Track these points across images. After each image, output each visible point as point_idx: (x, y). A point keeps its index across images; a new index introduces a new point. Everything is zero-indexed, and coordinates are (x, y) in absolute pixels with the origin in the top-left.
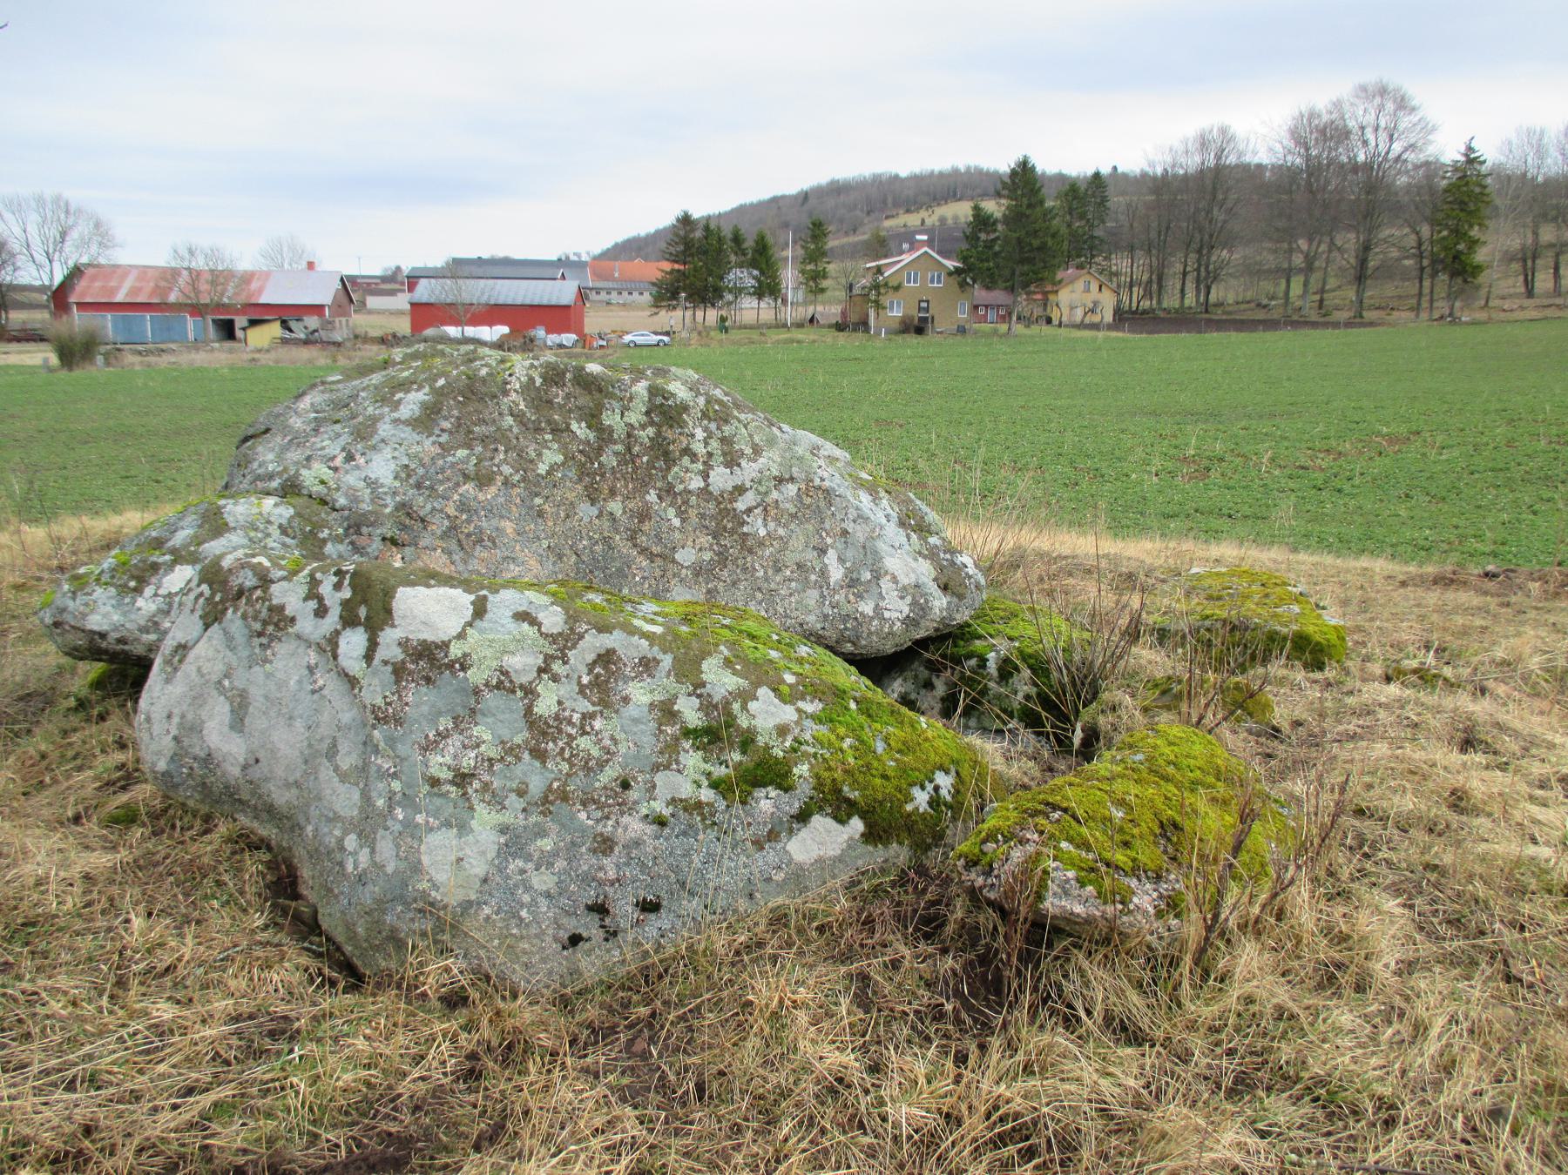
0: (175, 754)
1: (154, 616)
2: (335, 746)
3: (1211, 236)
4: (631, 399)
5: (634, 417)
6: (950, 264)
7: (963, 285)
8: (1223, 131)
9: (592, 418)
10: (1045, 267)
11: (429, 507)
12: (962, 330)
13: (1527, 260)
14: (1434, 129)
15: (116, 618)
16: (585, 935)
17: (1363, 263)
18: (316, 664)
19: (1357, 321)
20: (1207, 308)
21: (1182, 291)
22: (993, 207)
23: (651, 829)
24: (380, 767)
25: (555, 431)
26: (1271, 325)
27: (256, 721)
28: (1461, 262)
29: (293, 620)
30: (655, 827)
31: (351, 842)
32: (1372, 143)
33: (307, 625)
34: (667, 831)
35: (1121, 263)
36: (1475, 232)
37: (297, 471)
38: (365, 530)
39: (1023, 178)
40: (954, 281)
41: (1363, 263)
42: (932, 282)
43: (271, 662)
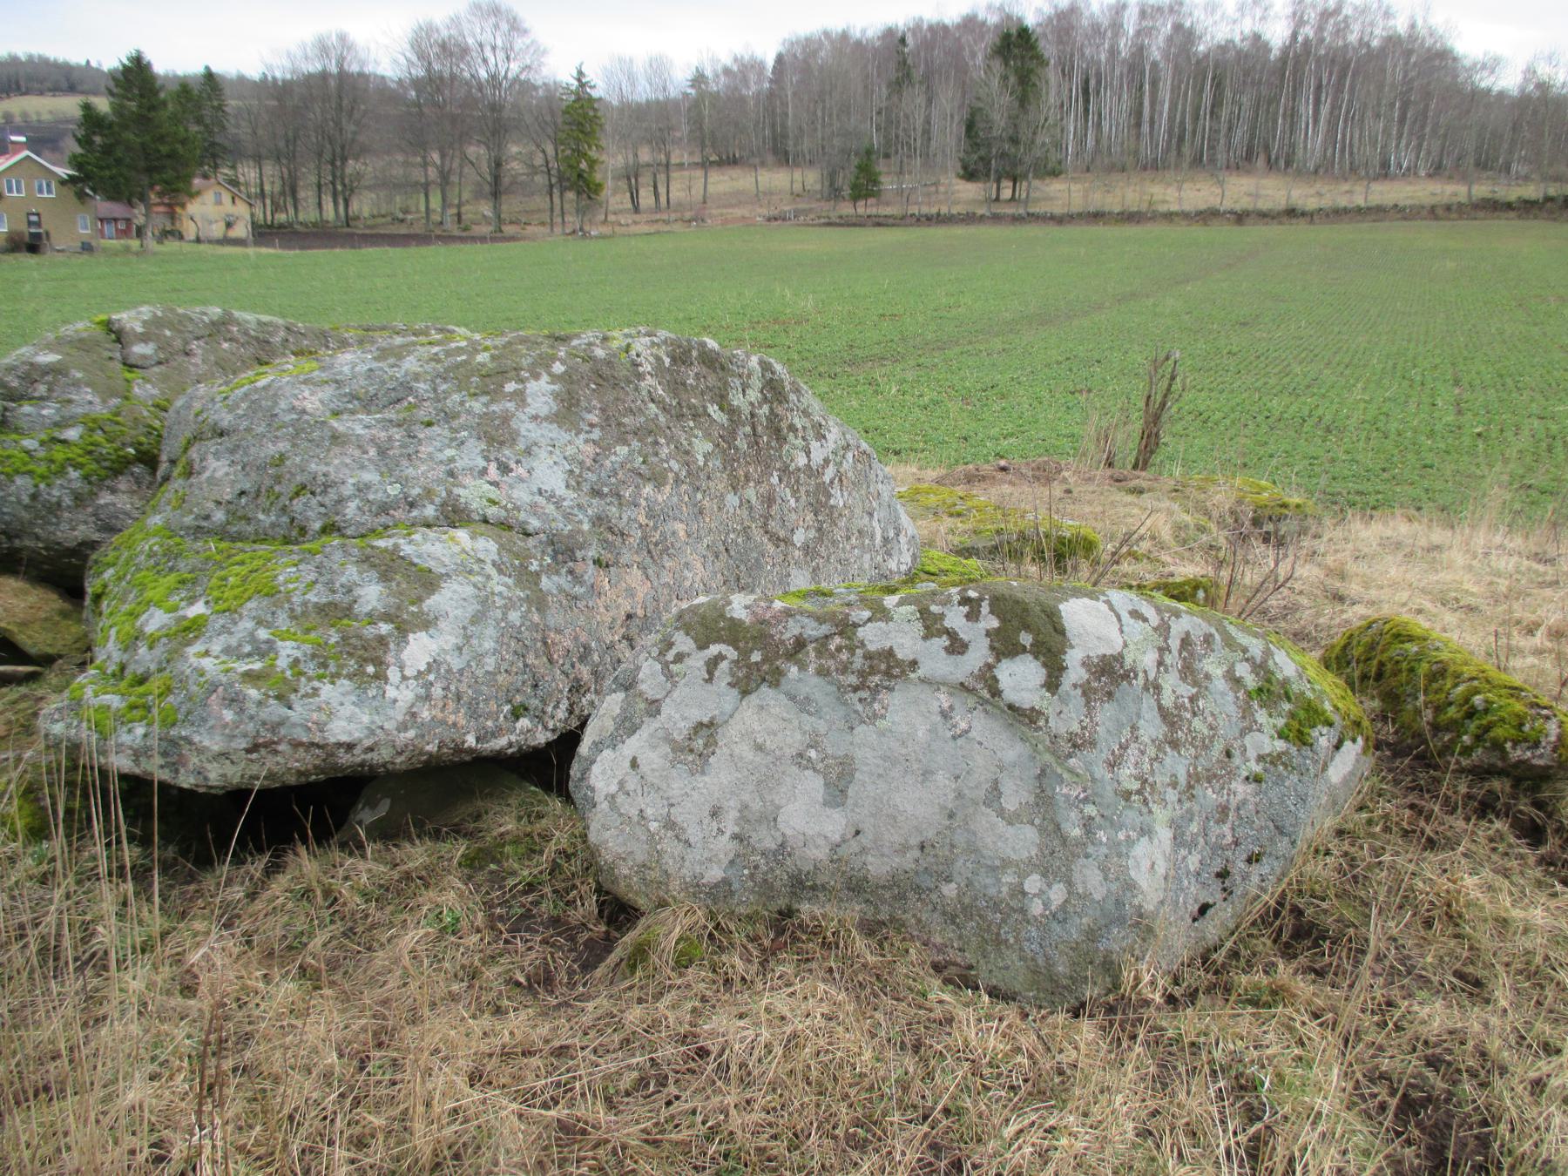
0: (737, 856)
1: (413, 705)
2: (996, 788)
3: (343, 148)
4: (749, 376)
5: (754, 395)
6: (63, 172)
7: (81, 196)
8: (342, 38)
9: (722, 400)
10: (178, 178)
11: (625, 517)
12: (87, 248)
13: (631, 176)
14: (545, 52)
15: (366, 719)
16: (1211, 901)
17: (497, 179)
18: (951, 708)
19: (498, 237)
20: (349, 221)
21: (320, 205)
22: (103, 105)
23: (1251, 787)
24: (1067, 796)
25: (695, 416)
26: (423, 239)
27: (864, 788)
28: (585, 180)
29: (914, 664)
30: (1253, 785)
31: (1033, 883)
32: (492, 61)
33: (934, 659)
34: (1264, 785)
35: (248, 173)
36: (593, 154)
37: (449, 493)
38: (579, 554)
39: (136, 74)
40: (69, 192)
41: (497, 179)
42: (41, 191)
43: (883, 717)
